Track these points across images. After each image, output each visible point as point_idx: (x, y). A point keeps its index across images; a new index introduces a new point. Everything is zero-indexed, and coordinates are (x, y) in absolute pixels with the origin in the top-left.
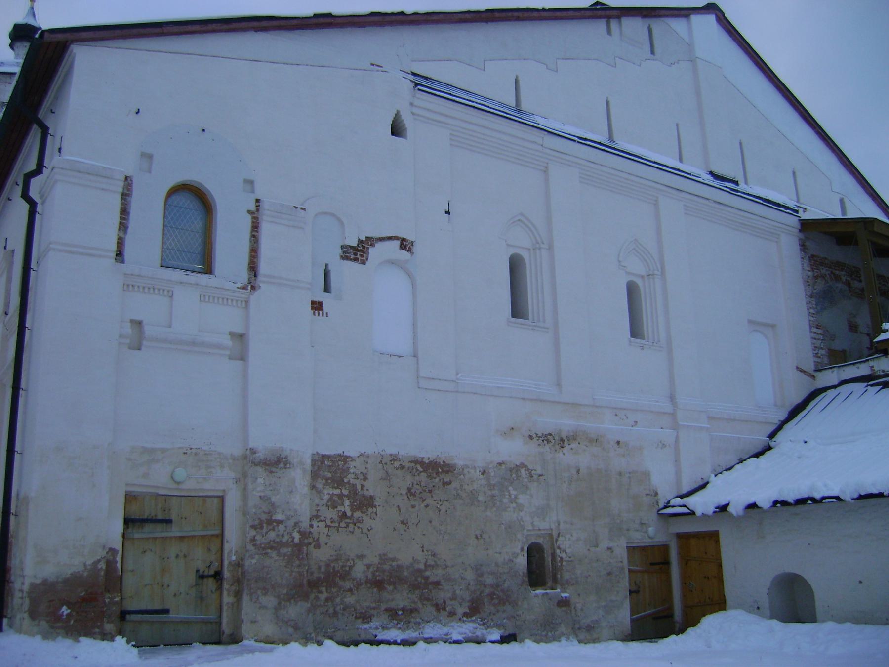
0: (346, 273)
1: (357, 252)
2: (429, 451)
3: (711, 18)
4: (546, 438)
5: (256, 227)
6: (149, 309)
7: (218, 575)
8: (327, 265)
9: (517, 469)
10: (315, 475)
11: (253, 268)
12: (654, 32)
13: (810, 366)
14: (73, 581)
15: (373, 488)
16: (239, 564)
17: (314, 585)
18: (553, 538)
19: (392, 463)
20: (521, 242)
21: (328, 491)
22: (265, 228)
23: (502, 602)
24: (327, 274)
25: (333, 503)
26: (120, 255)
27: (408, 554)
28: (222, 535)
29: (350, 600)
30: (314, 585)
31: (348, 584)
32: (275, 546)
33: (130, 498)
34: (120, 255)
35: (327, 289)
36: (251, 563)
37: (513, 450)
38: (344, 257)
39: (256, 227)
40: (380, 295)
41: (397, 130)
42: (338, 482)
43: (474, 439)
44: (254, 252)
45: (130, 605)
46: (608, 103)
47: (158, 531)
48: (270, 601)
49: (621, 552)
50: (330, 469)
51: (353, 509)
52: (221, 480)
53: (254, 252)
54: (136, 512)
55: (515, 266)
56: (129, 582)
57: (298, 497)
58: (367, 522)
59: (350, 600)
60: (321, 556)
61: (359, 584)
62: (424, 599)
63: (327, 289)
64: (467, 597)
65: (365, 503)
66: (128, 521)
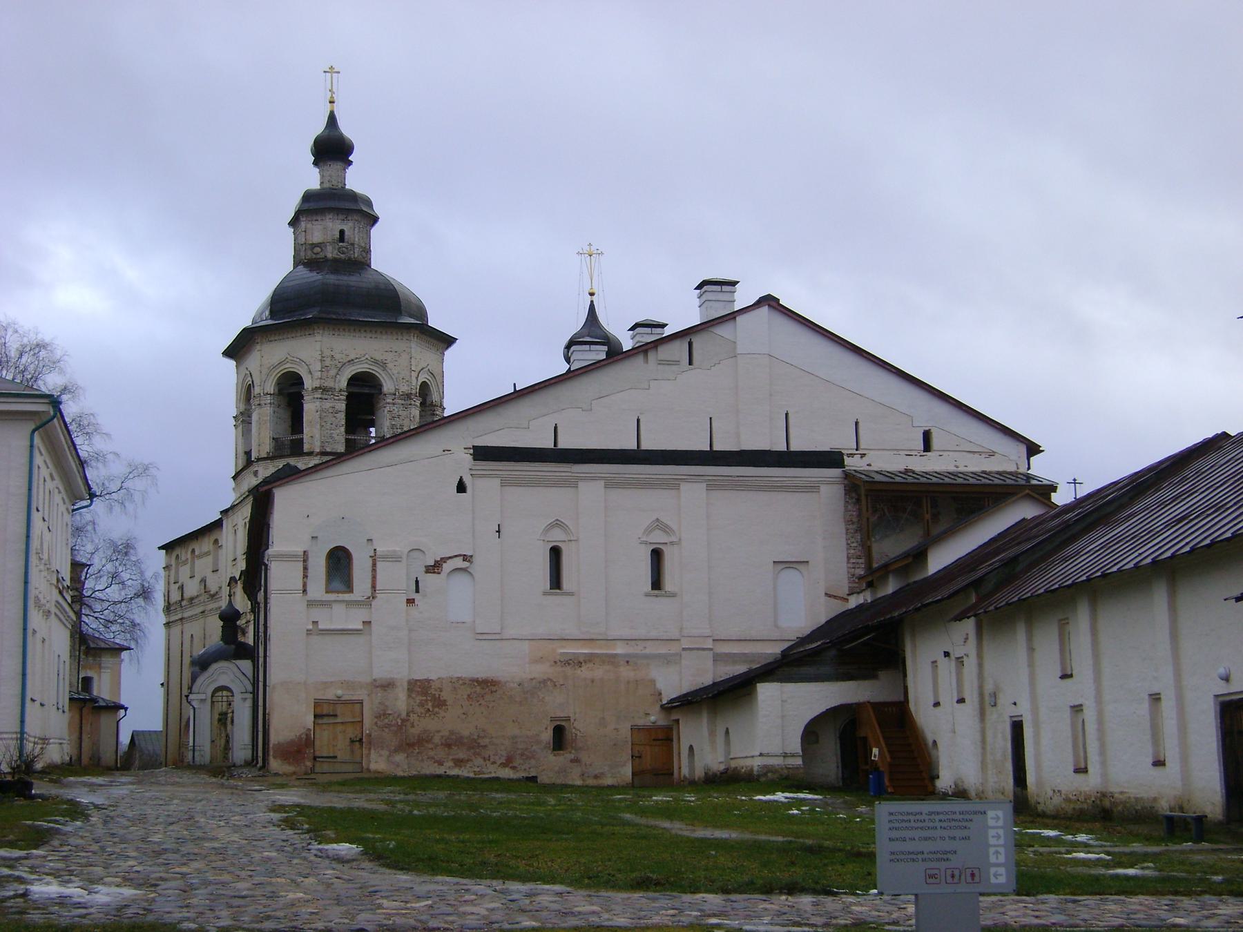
0: (429, 581)
1: (435, 568)
2: (482, 674)
3: (765, 310)
4: (567, 663)
5: (374, 565)
6: (320, 615)
7: (361, 740)
8: (332, 149)
9: (544, 682)
11: (374, 587)
12: (694, 345)
14: (292, 743)
15: (445, 695)
16: (370, 735)
17: (411, 745)
18: (568, 719)
19: (458, 683)
21: (419, 698)
22: (379, 565)
23: (528, 758)
24: (417, 582)
25: (421, 705)
26: (305, 591)
27: (466, 730)
29: (431, 753)
30: (411, 745)
31: (430, 746)
32: (388, 726)
33: (317, 704)
34: (305, 591)
35: (417, 591)
37: (542, 671)
38: (427, 572)
39: (374, 565)
40: (455, 598)
41: (461, 488)
42: (426, 694)
43: (509, 664)
44: (374, 578)
45: (318, 754)
46: (638, 421)
47: (332, 720)
48: (385, 753)
49: (625, 731)
50: (419, 688)
51: (433, 706)
52: (360, 694)
53: (374, 578)
54: (319, 711)
55: (556, 553)
56: (317, 743)
57: (400, 702)
58: (442, 713)
59: (431, 753)
60: (415, 731)
61: (437, 746)
62: (475, 754)
63: (417, 591)
64: (504, 753)
65: (440, 703)
66: (315, 716)
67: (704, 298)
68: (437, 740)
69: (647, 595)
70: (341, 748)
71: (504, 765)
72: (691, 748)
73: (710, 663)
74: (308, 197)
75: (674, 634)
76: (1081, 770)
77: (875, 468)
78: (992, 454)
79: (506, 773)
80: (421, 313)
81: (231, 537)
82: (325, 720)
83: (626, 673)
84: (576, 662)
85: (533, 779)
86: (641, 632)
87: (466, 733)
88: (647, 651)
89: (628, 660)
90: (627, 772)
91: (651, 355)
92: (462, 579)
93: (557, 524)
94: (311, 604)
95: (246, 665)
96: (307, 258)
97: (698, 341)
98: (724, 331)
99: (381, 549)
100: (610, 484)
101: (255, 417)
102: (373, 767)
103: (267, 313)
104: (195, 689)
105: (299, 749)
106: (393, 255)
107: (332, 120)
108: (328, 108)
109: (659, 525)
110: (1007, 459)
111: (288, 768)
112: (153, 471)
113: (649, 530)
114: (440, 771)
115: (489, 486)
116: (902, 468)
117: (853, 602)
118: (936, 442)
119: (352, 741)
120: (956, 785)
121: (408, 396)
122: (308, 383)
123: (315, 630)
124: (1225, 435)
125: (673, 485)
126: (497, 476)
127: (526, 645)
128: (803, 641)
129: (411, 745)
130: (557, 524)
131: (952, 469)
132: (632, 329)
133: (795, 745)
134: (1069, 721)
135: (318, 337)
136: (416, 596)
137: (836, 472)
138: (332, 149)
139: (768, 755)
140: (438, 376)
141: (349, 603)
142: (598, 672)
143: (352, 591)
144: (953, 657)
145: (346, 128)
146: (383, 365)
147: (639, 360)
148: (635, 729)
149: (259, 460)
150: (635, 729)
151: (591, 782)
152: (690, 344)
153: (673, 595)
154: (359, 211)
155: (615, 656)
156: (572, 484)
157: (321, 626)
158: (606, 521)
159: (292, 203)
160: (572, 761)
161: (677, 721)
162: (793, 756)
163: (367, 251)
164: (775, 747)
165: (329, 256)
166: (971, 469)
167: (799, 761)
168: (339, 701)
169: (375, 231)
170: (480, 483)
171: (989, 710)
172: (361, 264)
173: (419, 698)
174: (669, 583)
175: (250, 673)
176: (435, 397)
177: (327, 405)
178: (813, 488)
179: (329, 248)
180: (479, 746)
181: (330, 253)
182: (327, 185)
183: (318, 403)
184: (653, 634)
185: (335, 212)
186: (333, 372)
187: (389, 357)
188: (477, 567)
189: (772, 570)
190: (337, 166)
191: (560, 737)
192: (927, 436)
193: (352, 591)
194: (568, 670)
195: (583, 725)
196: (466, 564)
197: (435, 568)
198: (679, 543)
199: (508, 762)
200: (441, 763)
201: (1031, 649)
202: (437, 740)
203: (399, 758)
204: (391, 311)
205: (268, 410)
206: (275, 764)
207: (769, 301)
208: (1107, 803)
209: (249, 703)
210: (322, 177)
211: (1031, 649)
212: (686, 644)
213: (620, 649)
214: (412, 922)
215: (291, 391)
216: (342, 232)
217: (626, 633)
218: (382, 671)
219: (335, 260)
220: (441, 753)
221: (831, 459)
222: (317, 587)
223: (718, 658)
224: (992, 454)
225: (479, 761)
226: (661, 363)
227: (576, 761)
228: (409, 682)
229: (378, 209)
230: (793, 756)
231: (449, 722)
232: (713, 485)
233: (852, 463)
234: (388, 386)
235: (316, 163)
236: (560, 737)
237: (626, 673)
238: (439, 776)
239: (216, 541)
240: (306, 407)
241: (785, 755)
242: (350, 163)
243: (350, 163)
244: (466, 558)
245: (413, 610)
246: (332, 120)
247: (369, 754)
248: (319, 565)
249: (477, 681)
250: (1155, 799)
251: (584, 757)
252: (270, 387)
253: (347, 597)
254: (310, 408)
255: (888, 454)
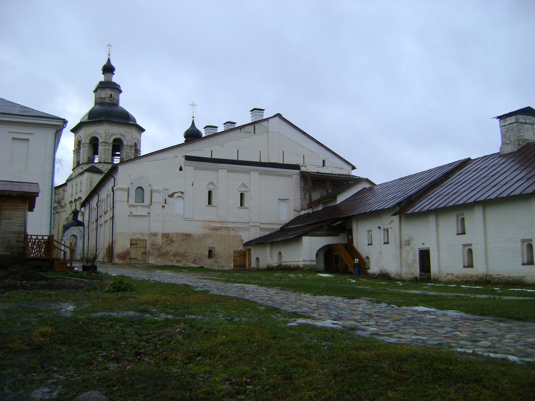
0: (169, 200)
1: (171, 196)
2: (186, 232)
4: (214, 229)
5: (151, 194)
8: (108, 69)
10: (163, 237)
11: (151, 201)
13: (299, 209)
14: (122, 253)
15: (174, 239)
16: (149, 251)
17: (162, 255)
18: (213, 248)
19: (178, 234)
20: (211, 187)
21: (165, 240)
22: (153, 194)
23: (201, 260)
25: (166, 242)
27: (181, 251)
28: (146, 247)
29: (169, 258)
30: (162, 255)
32: (155, 248)
33: (131, 240)
36: (151, 251)
37: (206, 231)
39: (151, 194)
40: (177, 206)
41: (181, 169)
43: (195, 229)
44: (151, 198)
48: (154, 257)
50: (166, 236)
53: (151, 198)
55: (210, 193)
56: (131, 254)
57: (159, 240)
58: (173, 245)
59: (169, 258)
60: (164, 250)
65: (172, 241)
67: (254, 114)
68: (171, 253)
69: (239, 208)
70: (139, 255)
71: (193, 263)
72: (258, 259)
73: (258, 231)
74: (101, 83)
75: (247, 221)
76: (471, 265)
77: (309, 171)
78: (342, 169)
79: (194, 265)
80: (134, 120)
81: (70, 188)
82: (134, 246)
83: (232, 233)
84: (217, 229)
85: (203, 267)
86: (237, 220)
87: (180, 252)
88: (239, 226)
89: (233, 229)
90: (232, 265)
91: (242, 129)
92: (180, 200)
93: (212, 183)
94: (130, 206)
95: (81, 228)
96: (99, 102)
97: (257, 126)
98: (265, 124)
99: (154, 188)
100: (229, 171)
101: (82, 150)
102: (150, 262)
103: (87, 117)
104: (65, 235)
105: (125, 256)
106: (126, 102)
107: (109, 60)
108: (108, 57)
109: (244, 185)
110: (345, 171)
111: (122, 262)
112: (62, 162)
113: (240, 187)
114: (172, 264)
115: (189, 169)
116: (316, 171)
117: (302, 213)
118: (326, 163)
119: (143, 253)
120: (381, 271)
121: (131, 146)
122: (100, 140)
123: (131, 215)
124: (469, 159)
125: (248, 172)
126: (191, 166)
127: (201, 223)
128: (287, 225)
129: (164, 255)
130: (212, 183)
131: (331, 172)
132: (205, 128)
133: (314, 258)
134: (461, 249)
135: (104, 126)
136: (165, 205)
137: (298, 171)
138: (108, 69)
139: (306, 261)
140: (139, 141)
141: (143, 206)
142: (224, 232)
143: (143, 202)
144: (382, 228)
145: (113, 63)
146: (124, 136)
147: (238, 131)
148: (235, 252)
149: (83, 164)
150: (235, 252)
151: (220, 269)
152: (254, 127)
153: (248, 208)
154: (117, 89)
155: (229, 227)
156: (217, 170)
157: (133, 214)
158: (228, 182)
159: (96, 83)
160: (215, 262)
161: (249, 250)
162: (313, 261)
163: (118, 101)
164: (308, 258)
165: (107, 102)
166: (336, 173)
167: (315, 263)
168: (138, 239)
169: (121, 95)
170: (188, 168)
171: (404, 247)
172: (116, 104)
173: (165, 240)
174: (246, 204)
175: (83, 231)
176: (138, 148)
177: (106, 147)
178: (291, 176)
179: (107, 99)
180: (185, 256)
181: (107, 101)
182: (106, 80)
183: (103, 147)
184: (241, 221)
185: (108, 88)
186: (108, 137)
187: (125, 134)
188: (185, 196)
189: (277, 202)
190: (109, 74)
191: (211, 254)
192: (324, 161)
193: (143, 202)
194: (214, 231)
195: (218, 250)
196: (182, 195)
197: (171, 196)
198: (249, 191)
199: (194, 262)
200: (172, 261)
201: (437, 225)
202: (171, 253)
203: (159, 259)
204: (126, 119)
205: (87, 148)
206: (116, 260)
207: (279, 115)
208: (488, 279)
209: (82, 240)
210: (105, 77)
211: (437, 225)
212: (251, 224)
213: (230, 225)
214: (340, 326)
215: (94, 143)
216: (111, 95)
217: (233, 220)
218: (153, 230)
219: (109, 103)
220: (172, 258)
221: (296, 167)
222: (132, 201)
223: (261, 229)
224: (342, 169)
225: (185, 261)
226: (245, 132)
227: (216, 261)
228: (162, 234)
229: (122, 89)
230: (313, 261)
231: (175, 248)
232: (261, 173)
233: (303, 169)
234: (125, 143)
235: (103, 74)
236: (211, 254)
237: (232, 233)
238: (172, 266)
239: (64, 190)
240: (100, 148)
241: (311, 261)
242: (114, 74)
243: (114, 74)
244: (182, 193)
245: (164, 210)
246: (109, 60)
247: (149, 258)
248: (133, 193)
249: (185, 234)
250: (523, 277)
251: (218, 260)
252: (88, 141)
253: (142, 204)
254: (101, 148)
255: (312, 167)
